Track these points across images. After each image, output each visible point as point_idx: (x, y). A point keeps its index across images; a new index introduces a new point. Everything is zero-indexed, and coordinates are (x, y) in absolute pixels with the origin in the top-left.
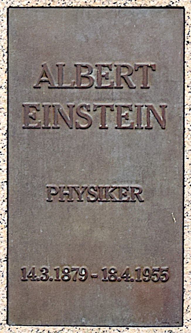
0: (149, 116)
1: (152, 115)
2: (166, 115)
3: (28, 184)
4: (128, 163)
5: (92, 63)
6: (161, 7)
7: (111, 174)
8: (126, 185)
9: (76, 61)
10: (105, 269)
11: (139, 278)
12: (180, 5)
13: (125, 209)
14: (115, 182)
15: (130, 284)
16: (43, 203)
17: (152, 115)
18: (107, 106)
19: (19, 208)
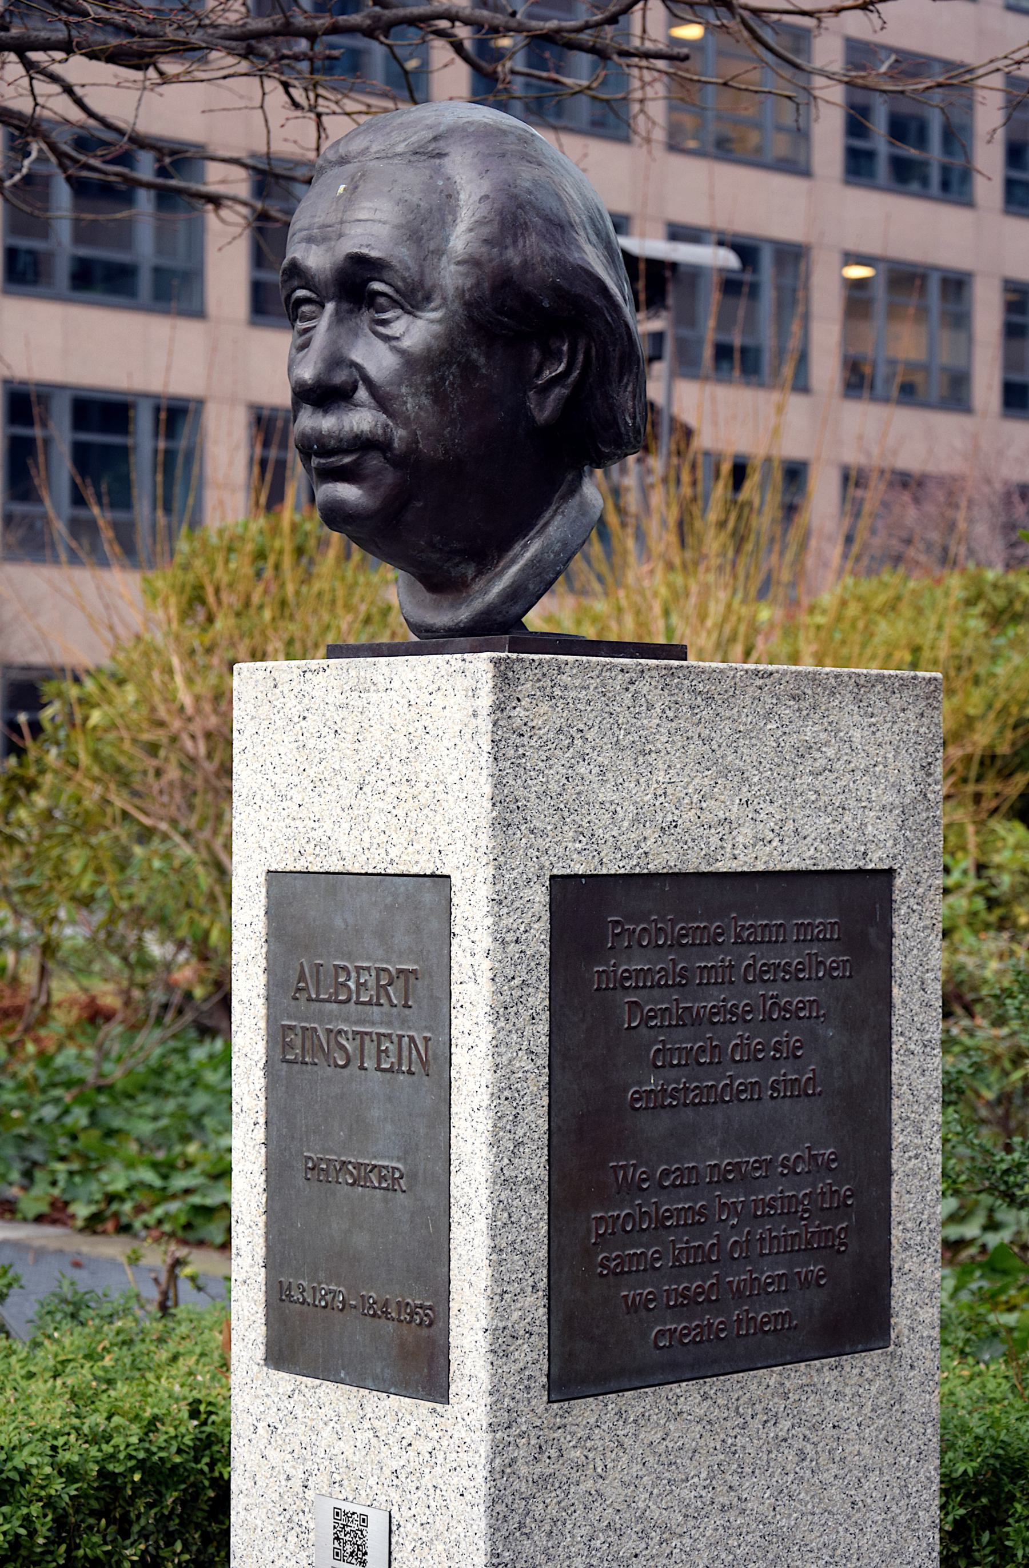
0: (410, 1053)
1: (414, 1052)
2: (430, 1053)
3: (115, 860)
4: (389, 1127)
5: (352, 962)
6: (425, 876)
7: (227, 15)
8: (386, 1163)
9: (335, 959)
10: (106, 980)
11: (399, 1315)
12: (445, 873)
13: (386, 1201)
14: (375, 1158)
15: (390, 1323)
16: (301, 1182)
17: (414, 1052)
18: (366, 1033)
19: (547, 1528)
